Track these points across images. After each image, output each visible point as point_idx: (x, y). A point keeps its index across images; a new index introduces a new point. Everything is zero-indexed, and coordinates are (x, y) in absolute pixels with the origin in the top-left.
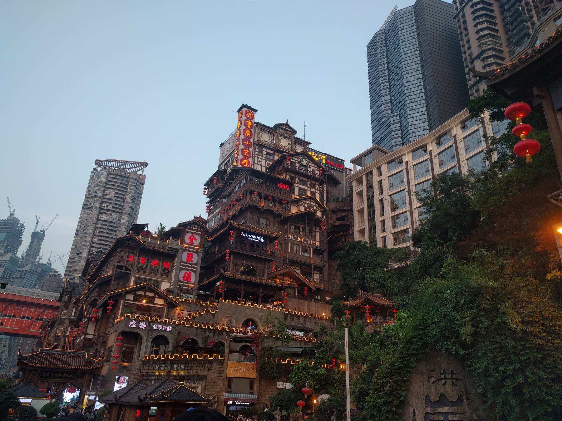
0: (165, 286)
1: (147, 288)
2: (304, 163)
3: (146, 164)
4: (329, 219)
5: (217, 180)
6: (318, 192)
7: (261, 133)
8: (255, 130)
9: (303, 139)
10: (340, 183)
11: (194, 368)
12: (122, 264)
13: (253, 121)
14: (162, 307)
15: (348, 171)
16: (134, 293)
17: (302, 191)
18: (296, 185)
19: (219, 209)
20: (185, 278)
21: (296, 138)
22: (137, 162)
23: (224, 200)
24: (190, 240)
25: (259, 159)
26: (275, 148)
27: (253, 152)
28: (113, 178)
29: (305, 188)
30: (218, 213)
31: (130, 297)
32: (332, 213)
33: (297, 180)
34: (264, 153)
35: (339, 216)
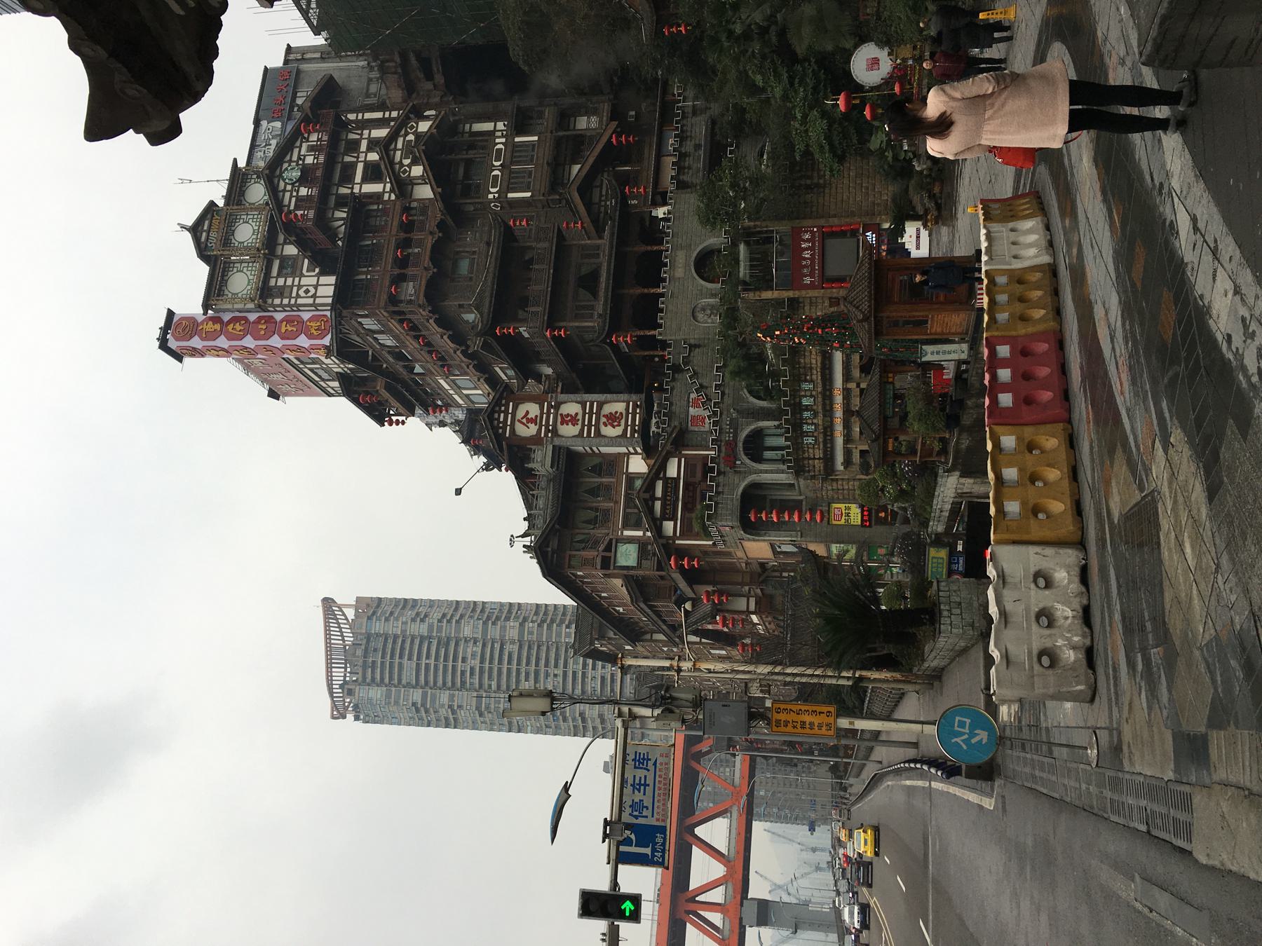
0: (638, 465)
1: (647, 496)
2: (294, 174)
3: (328, 603)
4: (431, 101)
5: (367, 393)
6: (366, 132)
7: (230, 295)
8: (225, 311)
9: (226, 186)
10: (331, 78)
11: (807, 360)
12: (599, 561)
13: (201, 318)
14: (683, 460)
15: (292, 57)
16: (658, 522)
17: (373, 173)
18: (356, 190)
19: (442, 382)
20: (616, 424)
21: (227, 204)
22: (325, 622)
23: (418, 369)
24: (529, 425)
25: (301, 293)
26: (264, 254)
27: (286, 311)
28: (373, 672)
29: (360, 167)
30: (451, 383)
31: (668, 527)
32: (414, 96)
33: (344, 191)
34: (281, 282)
35: (421, 75)
